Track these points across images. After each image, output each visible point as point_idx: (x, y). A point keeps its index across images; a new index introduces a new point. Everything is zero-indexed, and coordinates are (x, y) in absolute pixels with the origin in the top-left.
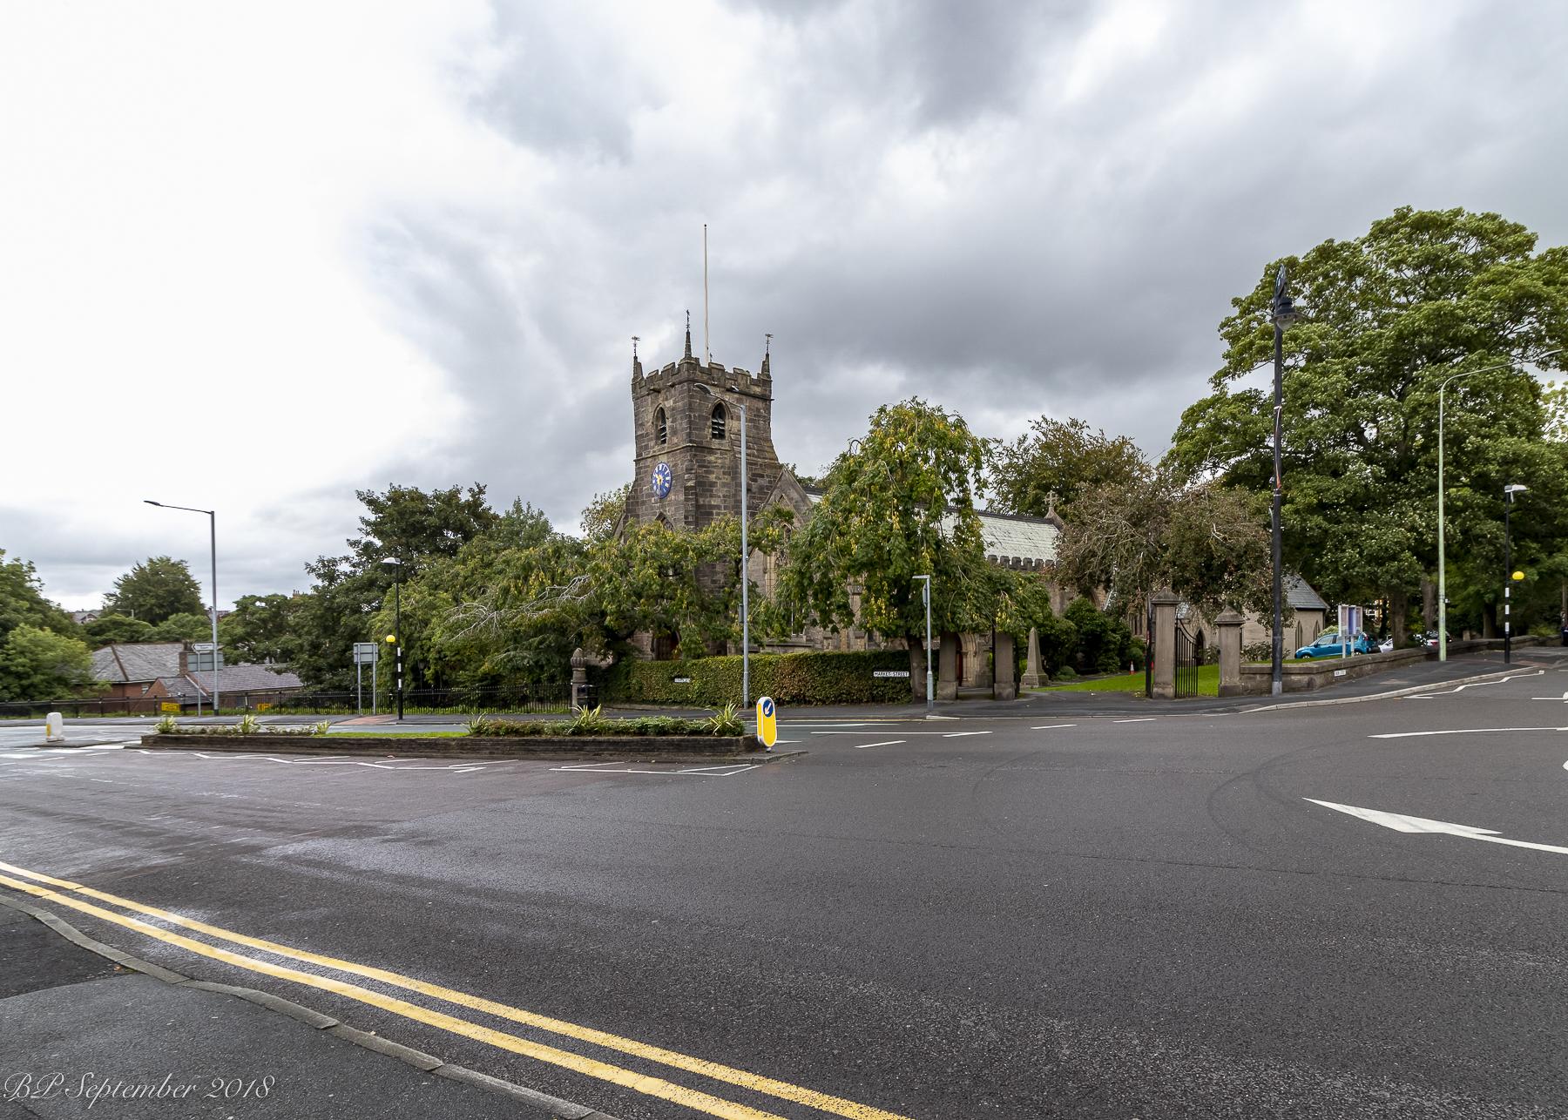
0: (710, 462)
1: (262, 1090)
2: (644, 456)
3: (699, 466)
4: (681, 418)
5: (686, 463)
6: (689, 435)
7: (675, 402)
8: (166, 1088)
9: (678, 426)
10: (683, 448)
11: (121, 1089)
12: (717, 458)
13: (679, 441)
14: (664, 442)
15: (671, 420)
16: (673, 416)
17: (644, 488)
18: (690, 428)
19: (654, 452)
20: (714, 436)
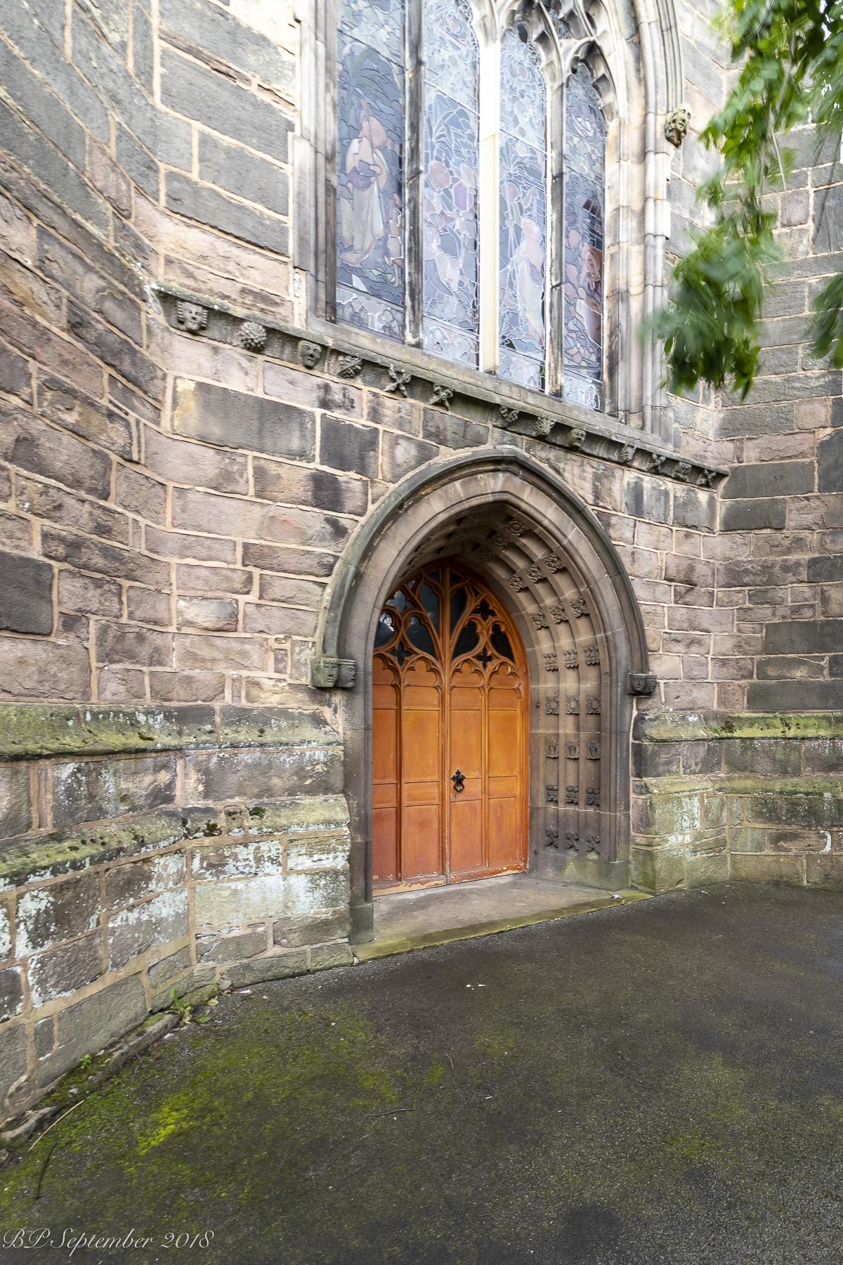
1: (204, 1243)
8: (129, 1240)
11: (94, 1242)
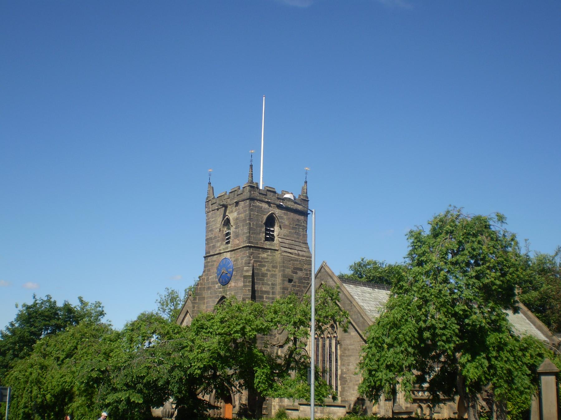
0: (263, 258)
2: (211, 253)
3: (255, 261)
4: (243, 226)
5: (245, 259)
6: (249, 238)
7: (239, 214)
9: (240, 231)
10: (243, 247)
12: (268, 255)
13: (239, 242)
14: (228, 243)
15: (234, 227)
16: (236, 224)
17: (210, 277)
18: (250, 232)
19: (220, 250)
20: (267, 239)
